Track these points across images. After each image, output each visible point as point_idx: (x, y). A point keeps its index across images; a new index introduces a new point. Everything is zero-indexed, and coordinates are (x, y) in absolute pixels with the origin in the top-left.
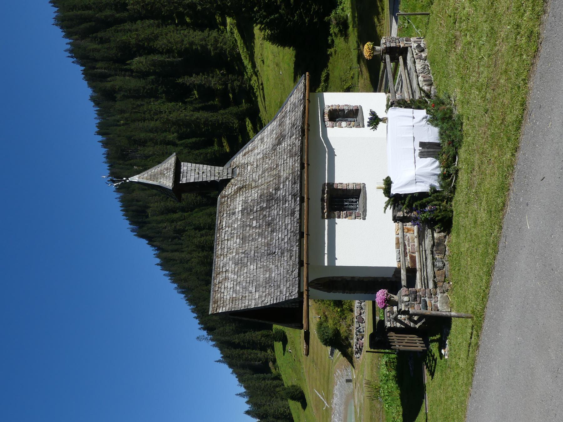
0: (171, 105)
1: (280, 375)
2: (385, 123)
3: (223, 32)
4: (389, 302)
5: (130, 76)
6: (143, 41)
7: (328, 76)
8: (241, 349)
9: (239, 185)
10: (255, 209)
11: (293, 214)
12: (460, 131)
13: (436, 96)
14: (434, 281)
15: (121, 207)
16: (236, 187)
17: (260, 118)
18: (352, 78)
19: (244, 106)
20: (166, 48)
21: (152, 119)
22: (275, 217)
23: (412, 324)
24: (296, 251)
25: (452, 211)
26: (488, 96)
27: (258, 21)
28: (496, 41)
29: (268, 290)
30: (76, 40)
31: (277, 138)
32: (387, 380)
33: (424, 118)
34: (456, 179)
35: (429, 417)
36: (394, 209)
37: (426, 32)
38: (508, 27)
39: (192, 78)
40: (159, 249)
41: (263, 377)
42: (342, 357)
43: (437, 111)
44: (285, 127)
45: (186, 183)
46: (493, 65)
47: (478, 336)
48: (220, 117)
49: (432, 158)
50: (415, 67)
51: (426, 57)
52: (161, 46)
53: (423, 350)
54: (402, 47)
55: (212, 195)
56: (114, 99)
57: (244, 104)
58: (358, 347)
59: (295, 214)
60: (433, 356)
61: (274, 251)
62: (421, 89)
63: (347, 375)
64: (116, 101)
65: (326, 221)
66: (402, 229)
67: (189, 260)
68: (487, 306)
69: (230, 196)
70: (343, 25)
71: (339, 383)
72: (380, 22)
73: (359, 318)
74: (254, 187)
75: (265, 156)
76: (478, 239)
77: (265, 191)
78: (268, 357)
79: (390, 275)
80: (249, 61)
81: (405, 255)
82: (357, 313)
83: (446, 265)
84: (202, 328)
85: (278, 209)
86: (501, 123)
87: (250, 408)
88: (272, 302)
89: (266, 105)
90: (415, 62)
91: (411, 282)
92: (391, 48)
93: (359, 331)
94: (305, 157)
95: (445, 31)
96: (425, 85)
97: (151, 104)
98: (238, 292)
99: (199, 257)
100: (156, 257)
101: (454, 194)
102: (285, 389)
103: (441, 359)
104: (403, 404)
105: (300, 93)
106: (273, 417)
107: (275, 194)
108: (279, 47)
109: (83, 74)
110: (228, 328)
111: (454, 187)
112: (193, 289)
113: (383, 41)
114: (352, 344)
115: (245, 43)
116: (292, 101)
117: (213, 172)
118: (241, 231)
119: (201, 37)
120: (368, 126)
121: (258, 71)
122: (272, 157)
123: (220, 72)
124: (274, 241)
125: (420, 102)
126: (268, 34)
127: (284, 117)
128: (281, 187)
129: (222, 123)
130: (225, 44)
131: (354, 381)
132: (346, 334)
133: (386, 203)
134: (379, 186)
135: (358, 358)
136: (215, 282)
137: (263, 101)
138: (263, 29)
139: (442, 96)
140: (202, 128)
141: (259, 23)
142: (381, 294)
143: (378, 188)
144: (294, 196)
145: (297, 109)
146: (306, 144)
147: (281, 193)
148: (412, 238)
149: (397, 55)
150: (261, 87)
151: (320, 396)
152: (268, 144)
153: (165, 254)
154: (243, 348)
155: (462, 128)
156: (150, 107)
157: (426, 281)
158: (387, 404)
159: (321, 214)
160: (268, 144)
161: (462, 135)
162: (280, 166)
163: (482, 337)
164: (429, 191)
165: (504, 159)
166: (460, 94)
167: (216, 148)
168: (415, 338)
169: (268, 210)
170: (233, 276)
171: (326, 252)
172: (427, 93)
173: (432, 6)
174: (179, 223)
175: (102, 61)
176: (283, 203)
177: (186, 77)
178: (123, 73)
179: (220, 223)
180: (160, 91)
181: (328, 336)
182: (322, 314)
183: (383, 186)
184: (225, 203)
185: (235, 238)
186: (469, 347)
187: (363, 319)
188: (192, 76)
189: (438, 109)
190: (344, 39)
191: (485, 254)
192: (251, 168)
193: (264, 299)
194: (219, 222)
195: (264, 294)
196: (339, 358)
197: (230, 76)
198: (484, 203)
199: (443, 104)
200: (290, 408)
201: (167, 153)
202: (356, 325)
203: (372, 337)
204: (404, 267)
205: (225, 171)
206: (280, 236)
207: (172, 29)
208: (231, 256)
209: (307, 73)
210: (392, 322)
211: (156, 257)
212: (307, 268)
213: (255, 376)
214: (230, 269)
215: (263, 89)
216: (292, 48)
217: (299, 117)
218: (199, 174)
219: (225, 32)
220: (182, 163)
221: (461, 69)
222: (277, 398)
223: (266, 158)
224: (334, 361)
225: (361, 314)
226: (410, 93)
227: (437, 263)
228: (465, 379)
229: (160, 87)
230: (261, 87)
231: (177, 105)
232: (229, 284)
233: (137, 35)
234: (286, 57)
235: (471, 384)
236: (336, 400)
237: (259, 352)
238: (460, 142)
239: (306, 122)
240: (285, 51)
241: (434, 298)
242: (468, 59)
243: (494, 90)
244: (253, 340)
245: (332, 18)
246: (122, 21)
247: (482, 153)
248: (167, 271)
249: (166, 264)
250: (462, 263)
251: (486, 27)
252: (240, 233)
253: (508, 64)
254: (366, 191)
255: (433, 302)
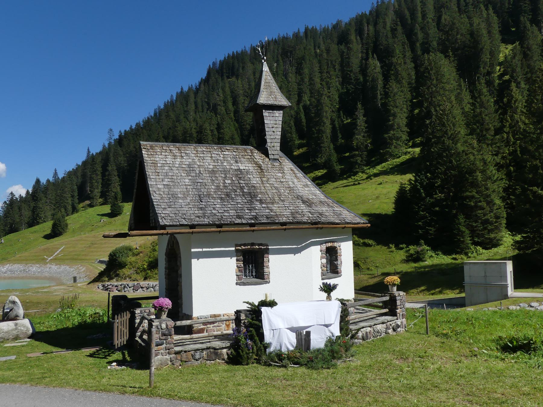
0: (336, 97)
1: (77, 212)
2: (327, 299)
3: (406, 144)
4: (159, 311)
5: (362, 57)
6: (396, 70)
7: (369, 245)
8: (102, 173)
9: (263, 166)
10: (242, 182)
11: (239, 217)
12: (322, 367)
13: (353, 344)
14: (182, 351)
15: (237, 51)
16: (262, 163)
17: (327, 183)
18: (368, 269)
19: (338, 168)
20: (390, 92)
21: (322, 80)
22: (235, 201)
23: (138, 334)
24: (204, 221)
25: (247, 364)
26: (354, 388)
27: (417, 177)
28: (403, 392)
29: (166, 196)
30: (394, 6)
31: (309, 200)
32: (80, 315)
33: (332, 333)
34: (277, 366)
35: (48, 355)
36: (248, 311)
37: (411, 332)
38: (415, 401)
39: (362, 116)
40: (198, 90)
41: (74, 195)
42: (99, 272)
43: (339, 345)
44: (319, 206)
45: (263, 116)
46: (382, 391)
47: (133, 393)
48: (326, 144)
49: (296, 343)
50: (379, 324)
51: (389, 334)
52: (391, 87)
53: (115, 345)
54: (397, 311)
55: (252, 140)
56: (340, 43)
57: (340, 167)
58: (109, 287)
59: (239, 219)
60: (109, 355)
61: (203, 201)
62: (358, 330)
63: (80, 278)
64: (338, 44)
65: (233, 249)
66: (229, 319)
67: (187, 119)
68: (163, 399)
69: (253, 158)
70: (416, 258)
71: (72, 270)
72: (421, 292)
73: (138, 287)
74: (262, 179)
75: (291, 189)
76: (224, 388)
77: (258, 191)
78: (95, 200)
79: (185, 311)
80: (380, 171)
81: (205, 324)
82: (143, 284)
83: (197, 362)
84: (122, 134)
85: (242, 203)
86: (330, 400)
87: (43, 183)
88: (154, 200)
89: (339, 189)
90: (383, 323)
91: (179, 330)
92: (395, 301)
93: (125, 287)
94: (292, 227)
95: (412, 349)
96: (363, 334)
97: (336, 78)
98: (163, 168)
99: (191, 128)
100: (189, 87)
101: (264, 365)
102: (63, 217)
103: (107, 363)
104: (58, 331)
105: (351, 219)
106: (34, 207)
107: (256, 200)
108: (395, 199)
109: (362, 13)
110: (122, 160)
111: (270, 365)
112: (159, 124)
113: (402, 293)
114: (112, 281)
115: (397, 166)
116: (344, 212)
117: (275, 141)
118: (220, 170)
119: (401, 124)
120: (323, 283)
121: (371, 179)
122: (291, 196)
123: (369, 143)
124: (213, 201)
125: (347, 330)
126: (406, 188)
127: (328, 205)
128: (263, 206)
129: (321, 147)
130: (395, 147)
131: (74, 284)
132: (121, 274)
133: (253, 303)
134: (268, 295)
135: (98, 288)
136: (171, 146)
137: (343, 185)
138: (411, 183)
139: (353, 349)
140: (315, 128)
141: (416, 178)
142: (167, 303)
143: (266, 295)
144: (255, 218)
145: (336, 217)
146: (304, 226)
147: (258, 205)
148: (221, 329)
149: (390, 307)
150: (356, 183)
151: (58, 252)
152: (302, 191)
153: (192, 96)
154: (103, 175)
155: (325, 368)
156: (334, 77)
157: (181, 344)
158: (57, 316)
159: (239, 243)
160: (302, 191)
161: (319, 369)
162: (282, 203)
163: (133, 397)
164: (265, 342)
165: (298, 405)
166: (356, 365)
167: (297, 142)
168: (126, 337)
169: (241, 194)
170: (177, 163)
171: (204, 250)
172: (355, 336)
173: (435, 337)
174: (223, 109)
175: (375, 31)
176: (249, 207)
177: (362, 111)
178: (365, 51)
179: (227, 149)
180: (349, 87)
181: (119, 257)
182: (141, 250)
183: (268, 300)
184: (246, 154)
185: (214, 164)
186: (122, 386)
187: (137, 290)
188: (364, 117)
189: (341, 346)
190: (404, 260)
191: (211, 395)
192: (280, 176)
193: (157, 193)
194: (228, 148)
195: (162, 193)
196: (97, 268)
197: (366, 153)
198: (257, 390)
199: (346, 351)
200: (44, 223)
201: (290, 95)
202: (131, 284)
203: (124, 297)
204: (193, 323)
205: (276, 152)
206: (218, 206)
207: (407, 97)
208: (196, 160)
209: (369, 225)
210: (140, 314)
211: (189, 87)
212: (189, 233)
213: (76, 187)
214: (184, 160)
215: (354, 185)
216: (393, 210)
217: (329, 220)
218: (272, 127)
219: (407, 147)
220: (282, 112)
221: (378, 365)
222: (54, 209)
223: (289, 191)
224: (93, 264)
225: (142, 288)
226: (355, 321)
227: (198, 354)
228: (91, 385)
229: (353, 87)
230: (356, 183)
231: (337, 103)
232: (169, 160)
233: (400, 64)
234: (385, 205)
235: (88, 390)
236: (54, 267)
237: (100, 190)
238: (312, 368)
239: (324, 226)
240: (391, 204)
241: (165, 353)
242: (387, 370)
243: (360, 392)
244: (111, 184)
245: (423, 247)
246: (413, 50)
247: (302, 387)
248: (176, 98)
249: (183, 97)
250: (200, 376)
251: (416, 383)
252: (218, 169)
253: (383, 402)
254: (263, 284)
255: (162, 351)
